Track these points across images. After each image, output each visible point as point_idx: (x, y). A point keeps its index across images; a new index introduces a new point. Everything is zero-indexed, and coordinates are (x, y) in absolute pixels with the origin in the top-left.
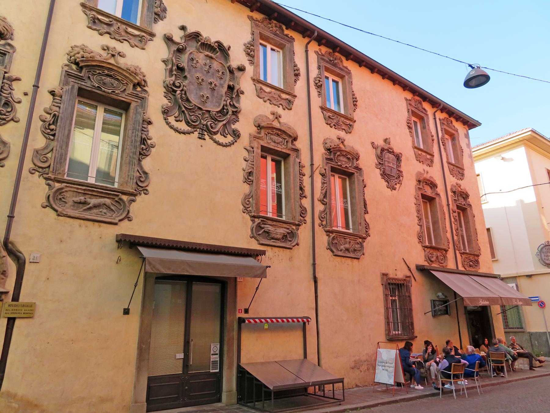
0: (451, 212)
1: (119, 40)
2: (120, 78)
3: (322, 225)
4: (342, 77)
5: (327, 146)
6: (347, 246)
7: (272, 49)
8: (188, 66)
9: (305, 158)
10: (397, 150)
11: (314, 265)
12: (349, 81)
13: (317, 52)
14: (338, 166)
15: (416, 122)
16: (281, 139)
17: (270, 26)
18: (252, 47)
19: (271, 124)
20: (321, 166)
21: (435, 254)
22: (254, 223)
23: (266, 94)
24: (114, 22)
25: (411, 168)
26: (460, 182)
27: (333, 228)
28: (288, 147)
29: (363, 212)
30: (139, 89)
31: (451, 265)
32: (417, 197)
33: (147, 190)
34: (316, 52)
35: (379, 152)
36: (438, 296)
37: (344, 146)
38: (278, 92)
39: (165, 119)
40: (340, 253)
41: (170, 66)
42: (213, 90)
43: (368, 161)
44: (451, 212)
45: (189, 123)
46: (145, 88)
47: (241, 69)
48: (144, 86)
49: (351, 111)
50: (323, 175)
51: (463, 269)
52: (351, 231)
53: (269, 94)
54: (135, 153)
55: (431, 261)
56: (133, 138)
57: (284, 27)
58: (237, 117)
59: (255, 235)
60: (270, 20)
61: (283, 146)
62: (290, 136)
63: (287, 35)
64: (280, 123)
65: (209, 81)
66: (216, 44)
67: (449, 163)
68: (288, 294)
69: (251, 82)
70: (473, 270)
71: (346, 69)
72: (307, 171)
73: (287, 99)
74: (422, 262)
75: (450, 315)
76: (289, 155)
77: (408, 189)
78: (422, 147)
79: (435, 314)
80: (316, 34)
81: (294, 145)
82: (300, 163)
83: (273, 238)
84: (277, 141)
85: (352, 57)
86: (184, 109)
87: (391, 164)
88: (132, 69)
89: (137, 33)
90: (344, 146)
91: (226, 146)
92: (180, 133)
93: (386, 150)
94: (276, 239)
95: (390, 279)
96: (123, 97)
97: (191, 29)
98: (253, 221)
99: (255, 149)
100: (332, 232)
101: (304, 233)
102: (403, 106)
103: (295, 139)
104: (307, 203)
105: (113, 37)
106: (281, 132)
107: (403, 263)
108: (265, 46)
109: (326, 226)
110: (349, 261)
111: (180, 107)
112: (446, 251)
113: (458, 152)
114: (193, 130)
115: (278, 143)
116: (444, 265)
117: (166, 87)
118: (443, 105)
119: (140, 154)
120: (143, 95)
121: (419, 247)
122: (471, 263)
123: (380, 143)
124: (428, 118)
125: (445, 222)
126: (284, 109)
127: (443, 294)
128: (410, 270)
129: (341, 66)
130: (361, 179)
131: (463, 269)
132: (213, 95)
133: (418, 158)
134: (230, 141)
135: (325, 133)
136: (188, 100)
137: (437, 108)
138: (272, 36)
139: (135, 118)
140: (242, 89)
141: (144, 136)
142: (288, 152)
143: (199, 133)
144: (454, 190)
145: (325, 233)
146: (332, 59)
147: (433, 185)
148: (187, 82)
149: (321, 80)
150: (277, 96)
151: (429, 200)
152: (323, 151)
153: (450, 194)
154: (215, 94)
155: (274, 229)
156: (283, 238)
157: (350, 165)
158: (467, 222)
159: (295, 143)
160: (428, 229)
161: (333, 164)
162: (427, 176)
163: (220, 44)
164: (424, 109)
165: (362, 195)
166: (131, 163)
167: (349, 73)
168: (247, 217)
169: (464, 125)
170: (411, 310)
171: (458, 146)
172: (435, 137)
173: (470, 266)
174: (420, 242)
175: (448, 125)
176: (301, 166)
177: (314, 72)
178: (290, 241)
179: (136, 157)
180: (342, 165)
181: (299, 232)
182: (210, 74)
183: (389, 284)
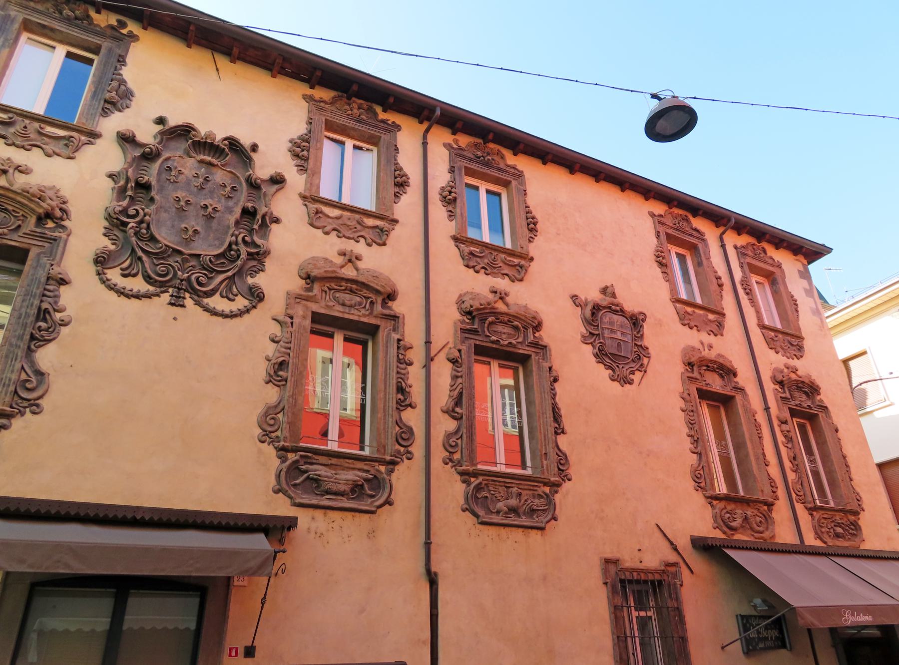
0: (776, 423)
1: (23, 147)
2: (10, 208)
3: (451, 460)
4: (506, 184)
5: (463, 306)
6: (513, 502)
7: (355, 147)
8: (158, 181)
9: (413, 332)
10: (630, 306)
11: (428, 544)
12: (518, 190)
13: (449, 144)
14: (493, 342)
15: (684, 256)
16: (358, 299)
17: (347, 107)
18: (304, 144)
19: (335, 272)
20: (451, 345)
21: (739, 511)
22: (283, 462)
23: (330, 220)
24: (16, 118)
25: (669, 341)
26: (795, 362)
27: (480, 467)
28: (375, 313)
29: (551, 430)
30: (50, 224)
31: (785, 534)
32: (685, 395)
33: (38, 406)
34: (447, 146)
35: (588, 313)
36: (755, 607)
37: (507, 305)
38: (357, 216)
39: (99, 274)
40: (495, 519)
41: (122, 183)
42: (210, 218)
43: (563, 332)
44: (776, 423)
45: (150, 278)
46: (63, 223)
47: (278, 181)
48: (62, 219)
49: (523, 242)
50: (454, 361)
51: (818, 543)
52: (529, 472)
53: (335, 221)
54: (21, 338)
55: (731, 528)
56: (23, 310)
57: (379, 109)
58: (262, 263)
59: (285, 486)
60: (349, 98)
61: (363, 311)
62: (378, 292)
63: (383, 121)
64: (357, 269)
65: (202, 204)
66: (226, 142)
67: (763, 327)
68: (362, 611)
69: (300, 202)
70: (846, 544)
71: (512, 170)
72: (417, 355)
73: (377, 227)
74: (706, 528)
75: (791, 650)
76: (377, 327)
77: (663, 382)
78: (699, 301)
79: (750, 648)
80: (438, 112)
81: (390, 308)
82: (399, 340)
83: (328, 492)
84: (348, 303)
85: (521, 146)
86: (140, 253)
87: (619, 334)
88: (31, 191)
89: (62, 133)
90: (507, 305)
91: (232, 316)
92: (128, 296)
93: (604, 307)
94: (336, 493)
95: (622, 570)
96: (14, 240)
97: (173, 122)
98: (283, 459)
99: (296, 321)
100: (476, 474)
101: (405, 480)
102: (647, 227)
103: (391, 296)
104: (413, 418)
105: (10, 142)
106: (358, 286)
107: (658, 534)
108: (477, 188)
109: (459, 463)
110: (518, 534)
111: (133, 250)
112: (770, 505)
113: (787, 306)
114: (158, 290)
115: (351, 306)
116: (766, 535)
117: (109, 217)
118: (736, 219)
119: (33, 337)
120: (57, 234)
121: (699, 499)
122: (839, 530)
123: (593, 295)
124: (707, 246)
125: (761, 444)
126: (369, 245)
127: (764, 601)
128: (676, 549)
129: (502, 166)
130: (546, 365)
131: (818, 543)
132: (208, 228)
133: (686, 320)
134: (241, 307)
135: (458, 282)
136: (153, 239)
137: (725, 225)
138: (351, 124)
139: (33, 275)
140: (276, 214)
141: (45, 306)
142: (373, 321)
143: (172, 296)
144: (780, 378)
145: (458, 477)
146: (479, 154)
147: (726, 371)
148: (153, 207)
149: (453, 190)
150: (354, 223)
151: (722, 402)
152: (457, 316)
153: (769, 387)
154: (214, 224)
155: (328, 474)
156: (353, 491)
157: (520, 340)
158: (822, 444)
159: (390, 303)
160: (816, 474)
161: (479, 340)
162: (712, 355)
163: (233, 144)
164: (696, 230)
165: (548, 397)
166: (11, 356)
167: (519, 175)
168: (270, 451)
169: (795, 255)
170: (684, 640)
171: (784, 294)
172: (725, 279)
173: (837, 536)
174: (699, 487)
175: (756, 257)
176: (402, 347)
177: (440, 176)
178: (372, 496)
179: (23, 345)
180: (499, 339)
181: (394, 477)
182: (204, 192)
183: (622, 581)
